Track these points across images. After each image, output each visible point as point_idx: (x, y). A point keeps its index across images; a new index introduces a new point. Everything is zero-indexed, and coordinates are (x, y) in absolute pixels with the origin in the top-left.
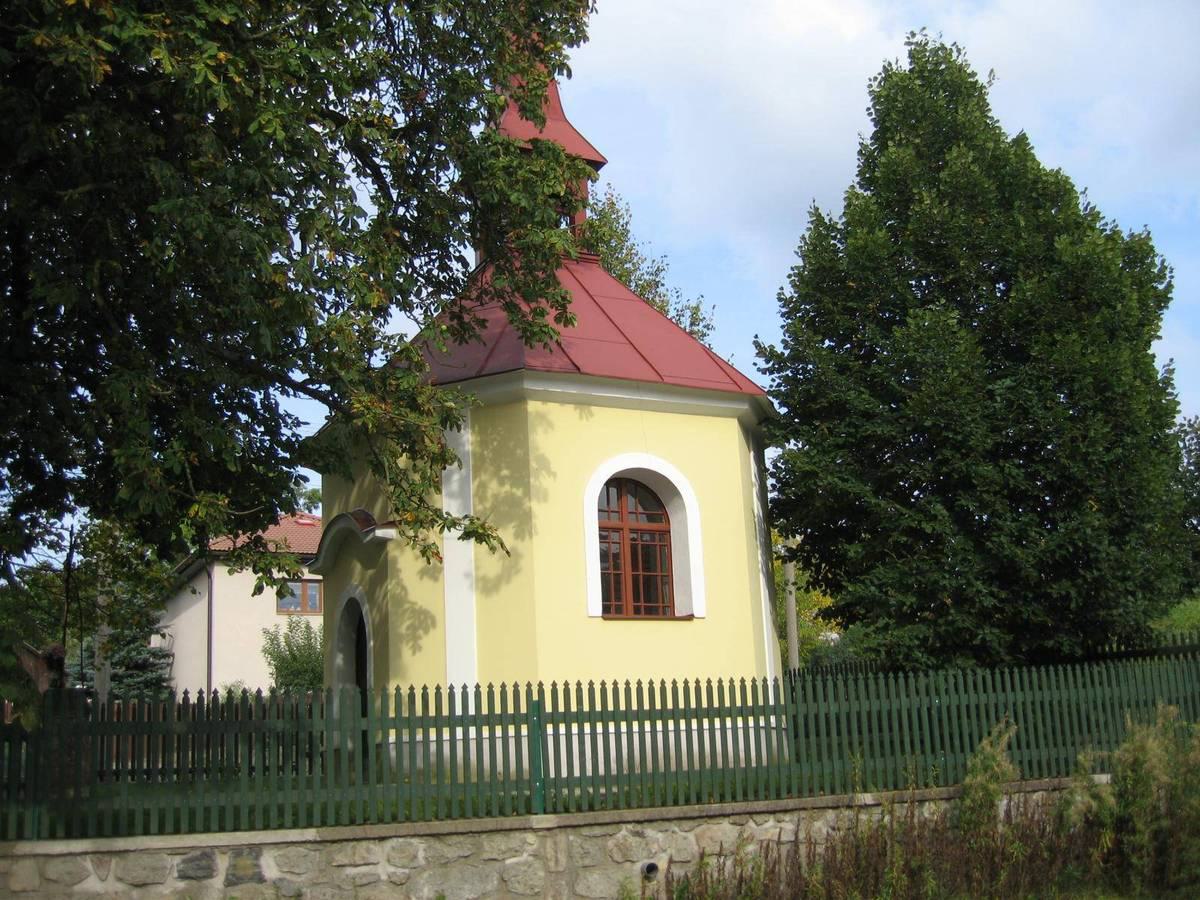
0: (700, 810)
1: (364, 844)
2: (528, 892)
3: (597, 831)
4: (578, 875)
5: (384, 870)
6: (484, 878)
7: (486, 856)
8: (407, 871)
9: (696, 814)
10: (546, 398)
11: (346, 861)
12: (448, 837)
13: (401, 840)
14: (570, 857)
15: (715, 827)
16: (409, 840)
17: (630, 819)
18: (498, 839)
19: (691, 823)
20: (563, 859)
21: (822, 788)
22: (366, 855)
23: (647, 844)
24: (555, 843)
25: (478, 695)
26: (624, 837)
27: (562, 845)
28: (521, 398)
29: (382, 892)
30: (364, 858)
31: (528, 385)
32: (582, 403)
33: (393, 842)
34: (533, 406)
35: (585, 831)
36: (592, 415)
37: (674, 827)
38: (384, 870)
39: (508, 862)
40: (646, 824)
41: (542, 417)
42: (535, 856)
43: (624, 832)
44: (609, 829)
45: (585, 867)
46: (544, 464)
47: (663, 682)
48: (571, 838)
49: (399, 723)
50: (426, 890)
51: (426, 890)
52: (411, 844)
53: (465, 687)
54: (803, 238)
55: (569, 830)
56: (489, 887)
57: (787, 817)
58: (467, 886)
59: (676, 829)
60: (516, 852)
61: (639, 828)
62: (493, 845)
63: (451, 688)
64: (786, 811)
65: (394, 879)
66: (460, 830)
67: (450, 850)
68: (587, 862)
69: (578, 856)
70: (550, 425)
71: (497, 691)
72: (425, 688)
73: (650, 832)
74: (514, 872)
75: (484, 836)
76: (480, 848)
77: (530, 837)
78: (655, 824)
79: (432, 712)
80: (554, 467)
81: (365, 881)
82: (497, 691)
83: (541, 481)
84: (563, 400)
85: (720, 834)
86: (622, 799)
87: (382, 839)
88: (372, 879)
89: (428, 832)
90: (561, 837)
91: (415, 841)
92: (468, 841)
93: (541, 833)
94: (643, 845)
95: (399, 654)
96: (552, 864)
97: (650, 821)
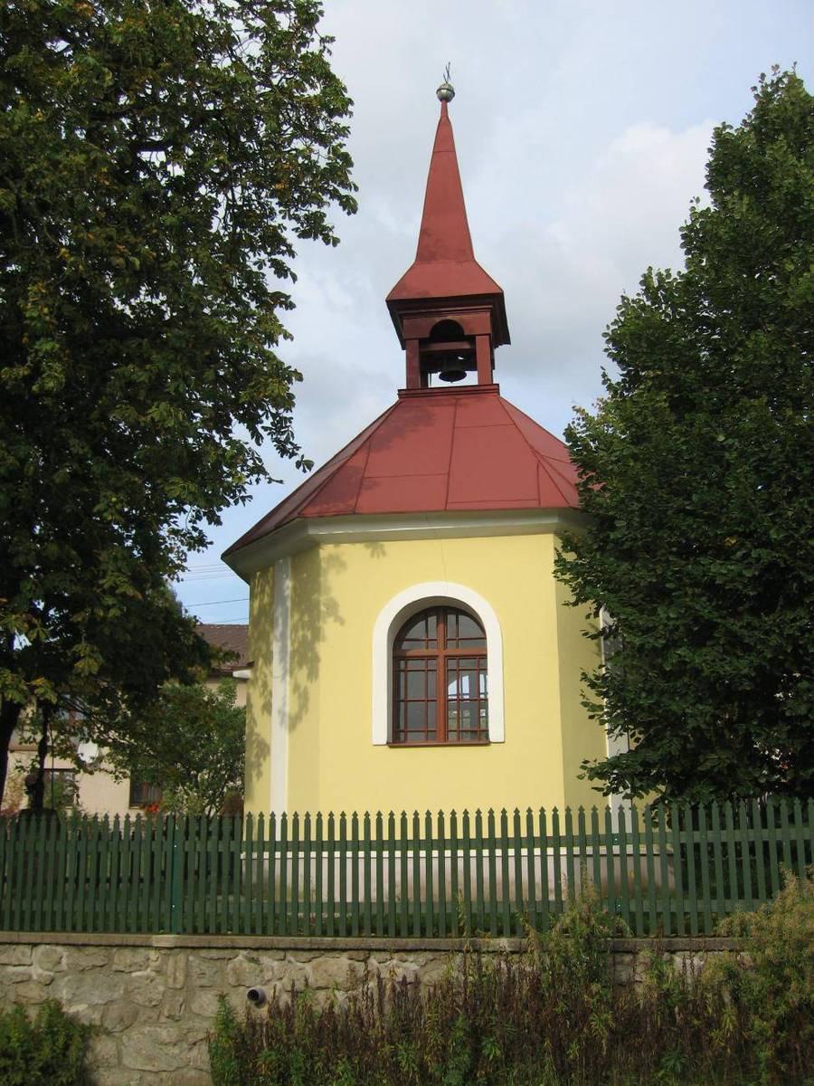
0: (385, 944)
1: (21, 948)
2: (147, 1004)
3: (214, 954)
4: (195, 993)
5: (36, 972)
6: (112, 987)
7: (115, 967)
8: (52, 974)
9: (308, 946)
10: (337, 541)
11: (6, 961)
12: (301, 953)
13: (48, 947)
14: (187, 976)
15: (332, 961)
16: (54, 947)
17: (242, 946)
18: (127, 952)
19: (307, 955)
20: (181, 977)
21: (373, 930)
22: (21, 958)
23: (261, 971)
24: (176, 962)
25: (367, 822)
26: (241, 962)
27: (181, 964)
28: (314, 545)
29: (31, 990)
30: (19, 960)
31: (312, 531)
32: (372, 540)
33: (41, 949)
34: (326, 551)
35: (204, 953)
36: (384, 553)
37: (290, 957)
38: (36, 972)
39: (134, 975)
40: (261, 952)
41: (335, 560)
42: (157, 972)
43: (240, 957)
44: (226, 953)
45: (201, 987)
46: (333, 607)
47: (491, 812)
48: (191, 958)
49: (250, 846)
50: (65, 992)
51: (65, 992)
52: (55, 951)
53: (416, 814)
54: (290, 367)
55: (189, 951)
56: (116, 996)
57: (411, 957)
58: (97, 993)
59: (292, 959)
60: (141, 967)
61: (254, 954)
62: (123, 958)
63: (273, 815)
64: (411, 951)
65: (42, 980)
66: (92, 943)
67: (96, 957)
68: (204, 982)
69: (195, 976)
70: (343, 565)
71: (422, 818)
72: (453, 813)
73: (266, 959)
74: (137, 984)
75: (115, 950)
76: (110, 959)
77: (153, 955)
78: (270, 953)
79: (435, 836)
80: (342, 612)
81: (19, 979)
82: (361, 819)
83: (329, 627)
84: (352, 540)
85: (335, 968)
86: (355, 925)
87: (135, 946)
88: (25, 978)
89: (66, 942)
90: (181, 957)
91: (60, 949)
92: (102, 952)
93: (163, 952)
94: (257, 972)
95: (251, 780)
96: (171, 981)
97: (266, 949)
